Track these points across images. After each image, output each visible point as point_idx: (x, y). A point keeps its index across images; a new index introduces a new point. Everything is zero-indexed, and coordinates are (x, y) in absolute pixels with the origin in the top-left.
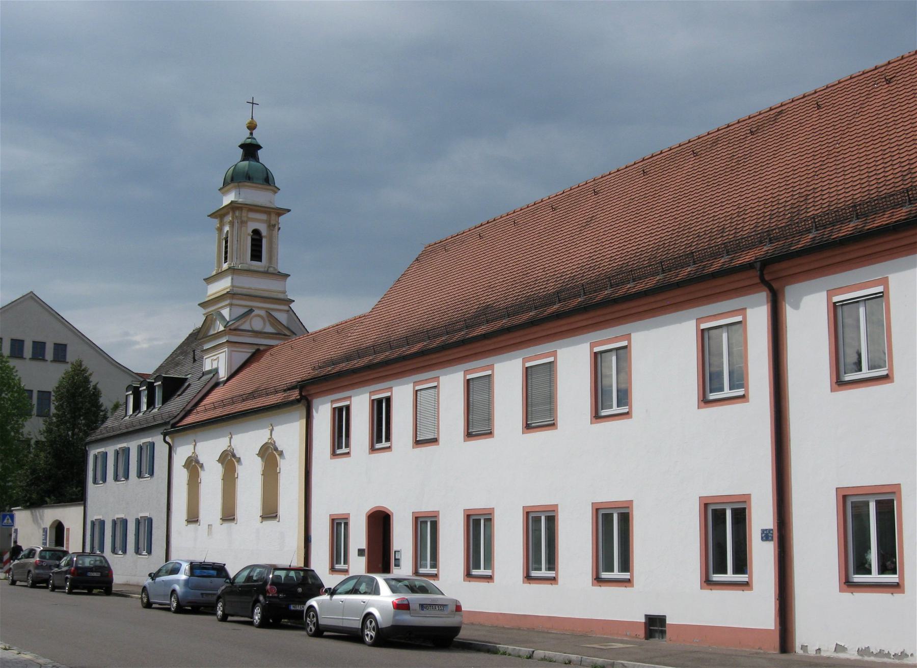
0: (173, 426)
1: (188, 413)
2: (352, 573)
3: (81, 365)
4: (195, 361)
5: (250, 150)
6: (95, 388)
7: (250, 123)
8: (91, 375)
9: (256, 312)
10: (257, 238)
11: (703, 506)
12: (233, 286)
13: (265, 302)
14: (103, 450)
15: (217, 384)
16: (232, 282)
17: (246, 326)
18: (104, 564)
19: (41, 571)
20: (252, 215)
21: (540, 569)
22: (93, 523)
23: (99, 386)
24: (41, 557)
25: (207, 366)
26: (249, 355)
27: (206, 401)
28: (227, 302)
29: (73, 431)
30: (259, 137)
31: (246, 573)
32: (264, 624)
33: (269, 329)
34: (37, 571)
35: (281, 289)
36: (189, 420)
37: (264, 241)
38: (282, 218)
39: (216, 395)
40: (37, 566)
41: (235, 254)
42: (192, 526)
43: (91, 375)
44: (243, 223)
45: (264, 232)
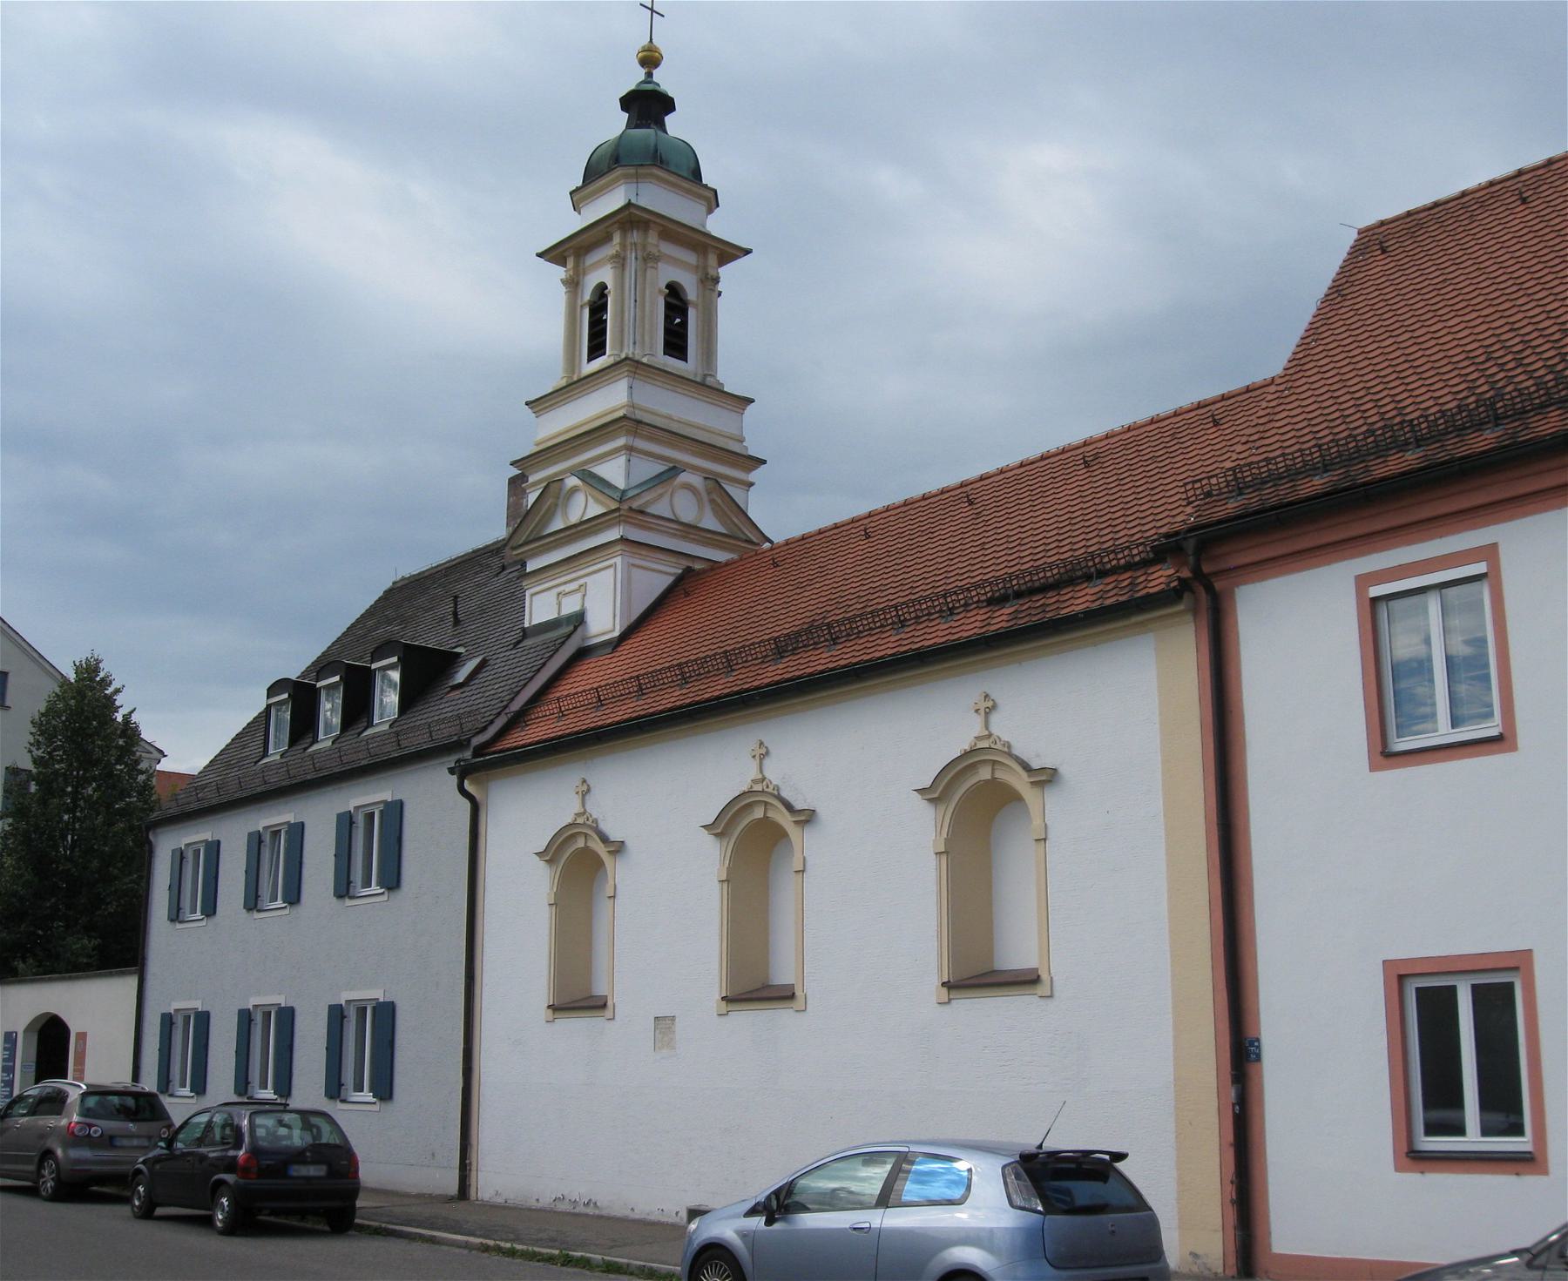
0: (479, 751)
2: (166, 1101)
3: (96, 670)
4: (457, 622)
5: (647, 105)
8: (118, 691)
9: (684, 477)
10: (676, 302)
11: (1395, 980)
12: (632, 406)
14: (290, 817)
15: (583, 653)
16: (631, 394)
17: (661, 508)
18: (327, 1137)
20: (667, 248)
21: (1460, 1130)
22: (168, 1021)
23: (134, 718)
24: (86, 1112)
25: (541, 607)
26: (670, 580)
28: (621, 442)
29: (74, 812)
30: (664, 79)
31: (204, 1118)
32: (232, 1229)
33: (710, 522)
34: (74, 1153)
35: (733, 431)
37: (692, 314)
38: (727, 273)
40: (74, 1139)
41: (629, 329)
43: (118, 691)
44: (649, 259)
45: (691, 292)
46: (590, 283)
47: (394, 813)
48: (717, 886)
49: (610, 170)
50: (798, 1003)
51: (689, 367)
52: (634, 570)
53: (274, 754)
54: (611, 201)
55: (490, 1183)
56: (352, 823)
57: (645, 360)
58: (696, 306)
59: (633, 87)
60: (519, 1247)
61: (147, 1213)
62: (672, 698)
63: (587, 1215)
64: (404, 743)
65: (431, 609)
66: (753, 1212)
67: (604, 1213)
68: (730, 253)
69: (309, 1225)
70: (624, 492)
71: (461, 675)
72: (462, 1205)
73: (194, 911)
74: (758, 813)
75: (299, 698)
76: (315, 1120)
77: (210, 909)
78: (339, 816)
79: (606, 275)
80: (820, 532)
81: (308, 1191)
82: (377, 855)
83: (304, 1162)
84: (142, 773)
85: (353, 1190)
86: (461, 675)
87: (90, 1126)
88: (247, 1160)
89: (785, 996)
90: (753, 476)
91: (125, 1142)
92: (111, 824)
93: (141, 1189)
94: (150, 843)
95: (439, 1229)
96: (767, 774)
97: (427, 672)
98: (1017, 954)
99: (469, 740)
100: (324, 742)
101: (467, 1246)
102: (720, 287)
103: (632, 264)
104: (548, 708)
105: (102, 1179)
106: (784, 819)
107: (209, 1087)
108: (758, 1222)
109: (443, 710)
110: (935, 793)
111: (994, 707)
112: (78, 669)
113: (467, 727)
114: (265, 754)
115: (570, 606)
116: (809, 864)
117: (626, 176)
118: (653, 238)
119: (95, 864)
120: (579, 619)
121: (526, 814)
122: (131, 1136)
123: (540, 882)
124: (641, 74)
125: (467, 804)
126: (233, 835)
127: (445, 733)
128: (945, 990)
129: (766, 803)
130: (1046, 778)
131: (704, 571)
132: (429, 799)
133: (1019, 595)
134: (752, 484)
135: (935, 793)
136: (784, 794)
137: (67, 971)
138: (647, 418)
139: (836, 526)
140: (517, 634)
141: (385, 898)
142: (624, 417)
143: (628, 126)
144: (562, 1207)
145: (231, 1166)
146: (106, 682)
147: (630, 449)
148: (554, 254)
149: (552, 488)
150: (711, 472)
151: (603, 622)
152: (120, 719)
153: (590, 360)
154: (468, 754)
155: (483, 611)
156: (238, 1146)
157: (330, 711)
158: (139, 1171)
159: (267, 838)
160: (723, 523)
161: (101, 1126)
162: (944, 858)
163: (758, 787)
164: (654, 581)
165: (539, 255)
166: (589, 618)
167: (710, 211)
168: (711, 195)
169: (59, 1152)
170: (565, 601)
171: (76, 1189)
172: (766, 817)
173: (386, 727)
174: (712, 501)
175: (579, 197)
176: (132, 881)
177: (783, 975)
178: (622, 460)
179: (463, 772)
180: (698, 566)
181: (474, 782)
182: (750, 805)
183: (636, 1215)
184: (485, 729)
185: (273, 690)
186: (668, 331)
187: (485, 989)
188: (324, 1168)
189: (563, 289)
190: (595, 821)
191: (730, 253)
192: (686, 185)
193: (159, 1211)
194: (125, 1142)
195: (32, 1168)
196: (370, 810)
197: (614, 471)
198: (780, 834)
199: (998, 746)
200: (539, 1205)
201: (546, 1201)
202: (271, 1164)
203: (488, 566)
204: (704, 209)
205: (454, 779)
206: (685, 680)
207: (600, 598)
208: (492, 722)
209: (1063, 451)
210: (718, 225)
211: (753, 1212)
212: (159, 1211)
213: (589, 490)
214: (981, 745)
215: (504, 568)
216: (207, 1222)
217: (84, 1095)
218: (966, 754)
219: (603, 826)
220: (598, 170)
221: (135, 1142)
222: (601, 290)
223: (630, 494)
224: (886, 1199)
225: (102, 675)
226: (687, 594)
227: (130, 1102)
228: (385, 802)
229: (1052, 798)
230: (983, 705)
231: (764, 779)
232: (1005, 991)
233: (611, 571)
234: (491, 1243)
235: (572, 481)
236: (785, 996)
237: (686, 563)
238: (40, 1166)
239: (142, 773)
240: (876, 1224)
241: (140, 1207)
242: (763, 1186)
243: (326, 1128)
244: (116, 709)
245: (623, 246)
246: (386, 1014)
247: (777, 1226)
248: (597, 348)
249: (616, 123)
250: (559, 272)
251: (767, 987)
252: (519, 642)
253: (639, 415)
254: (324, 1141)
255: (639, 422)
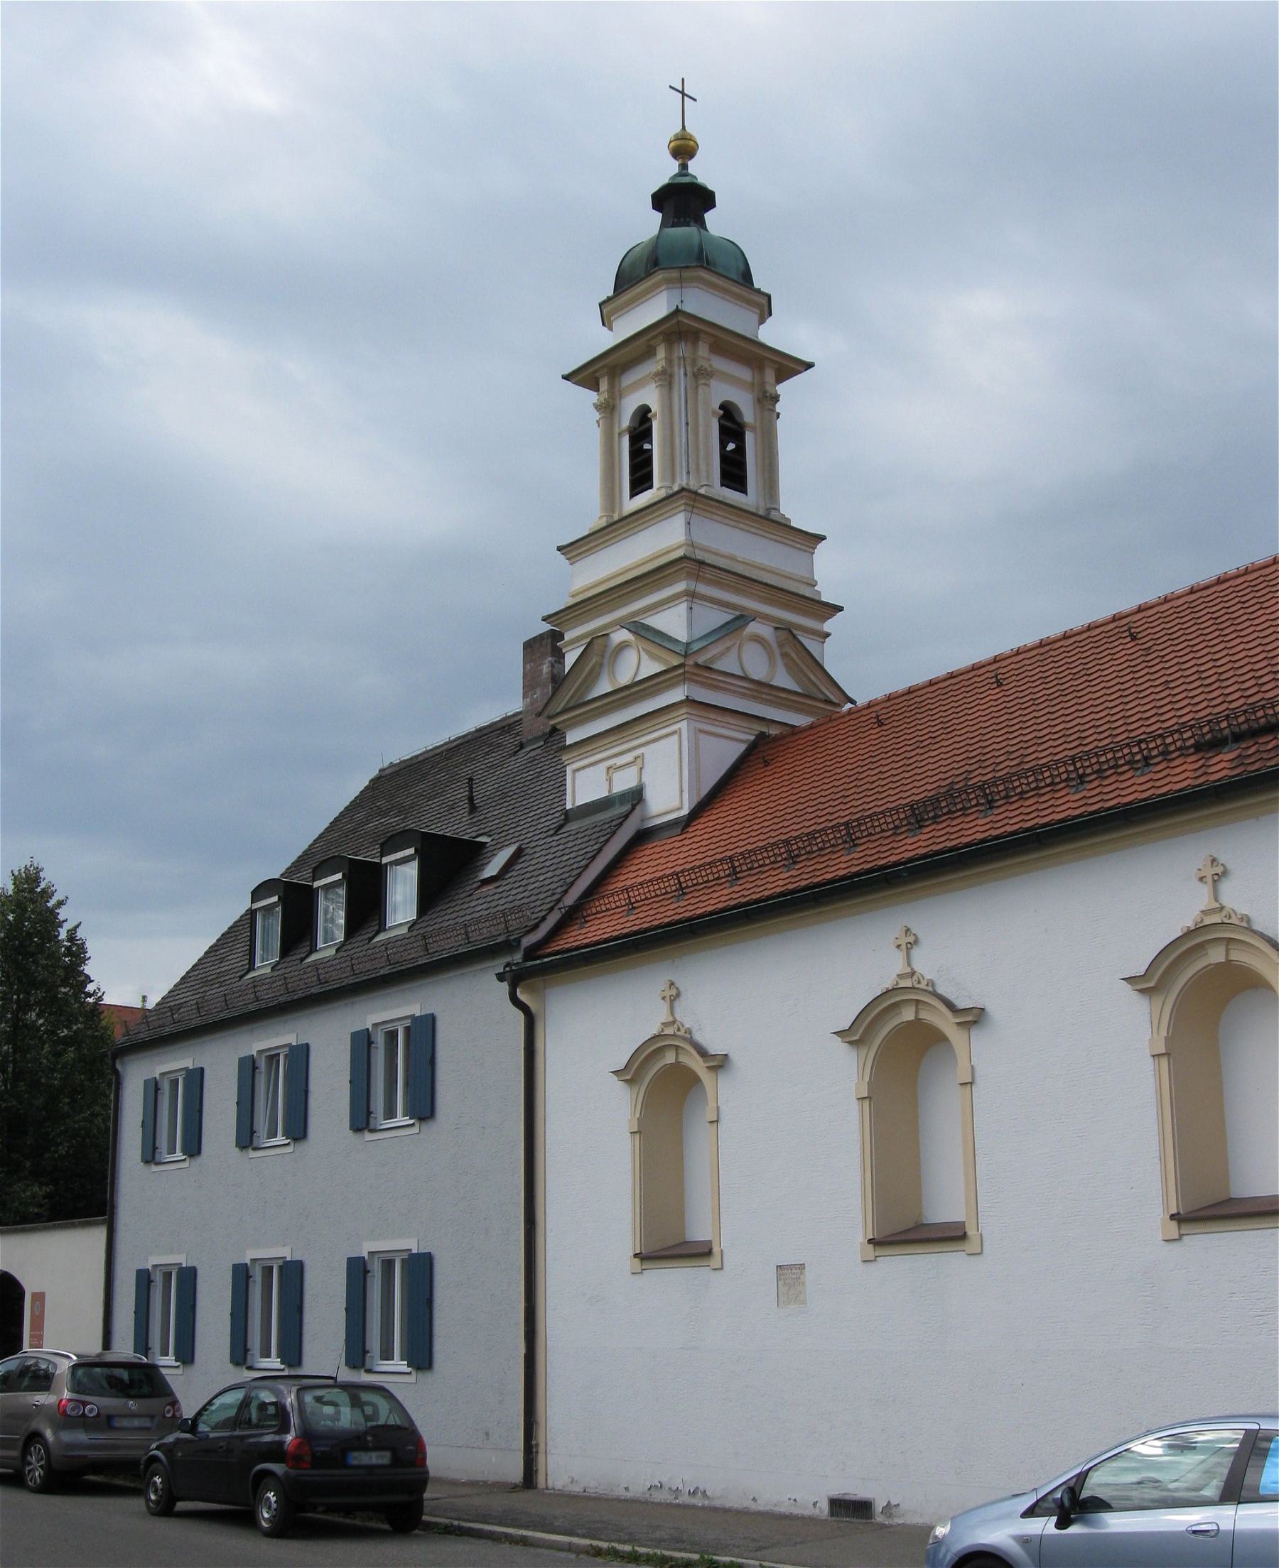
0: (531, 953)
1: (572, 916)
4: (473, 808)
5: (684, 201)
6: (72, 936)
7: (677, 138)
8: (60, 904)
9: (754, 628)
10: (731, 425)
12: (692, 545)
13: (771, 602)
14: (188, 1063)
17: (728, 664)
18: (385, 1415)
19: (82, 1437)
20: (719, 364)
22: (144, 1279)
23: (80, 934)
24: (77, 1387)
25: (587, 784)
27: (627, 877)
28: (681, 586)
30: (702, 170)
32: (282, 1530)
33: (783, 679)
34: (67, 1437)
36: (601, 927)
39: (650, 865)
40: (64, 1419)
42: (674, 1279)
43: (60, 904)
44: (701, 375)
45: (748, 414)
46: (629, 407)
47: (423, 1033)
48: (1149, 1064)
49: (648, 275)
50: (972, 1246)
51: (750, 499)
52: (702, 736)
53: (264, 966)
54: (653, 309)
55: (565, 1466)
56: (370, 1043)
57: (702, 491)
58: (753, 429)
59: (666, 181)
60: (642, 1550)
61: (165, 1509)
62: (778, 881)
63: (694, 1507)
64: (474, 937)
65: (435, 796)
66: (1030, 1513)
67: (717, 1503)
68: (790, 367)
69: (358, 1522)
70: (688, 644)
71: (491, 870)
72: (528, 1495)
73: (172, 1150)
74: (670, 1058)
75: (292, 901)
76: (365, 1397)
77: (193, 1147)
78: (146, 1082)
79: (650, 396)
80: (931, 683)
81: (366, 1479)
82: (406, 1079)
83: (365, 1449)
84: (90, 995)
85: (421, 1481)
86: (491, 870)
87: (85, 1404)
88: (299, 1446)
89: (701, 1253)
90: (828, 626)
91: (125, 1423)
92: (58, 1055)
93: (158, 1480)
94: (117, 1073)
95: (527, 1528)
96: (917, 966)
97: (447, 867)
98: (945, 1207)
99: (518, 941)
100: (325, 950)
101: (570, 1548)
102: (779, 407)
103: (681, 381)
104: (613, 899)
105: (98, 1466)
106: (697, 1064)
107: (197, 1356)
108: (1045, 1526)
109: (475, 909)
110: (1149, 983)
111: (1225, 873)
112: (16, 880)
113: (514, 925)
114: (251, 967)
115: (624, 782)
116: (722, 1116)
117: (668, 281)
118: (703, 350)
119: (40, 1102)
120: (636, 797)
121: (593, 1030)
122: (133, 1415)
123: (618, 1109)
124: (673, 167)
125: (520, 1016)
126: (219, 1061)
127: (483, 935)
128: (1174, 1223)
129: (677, 1047)
130: (974, 1018)
131: (776, 739)
132: (470, 1015)
133: (1238, 737)
134: (828, 635)
135: (1149, 983)
136: (941, 990)
137: (15, 1223)
138: (709, 559)
139: (952, 676)
140: (558, 818)
141: (415, 1130)
142: (683, 558)
143: (664, 224)
144: (659, 1497)
145: (276, 1453)
146: (47, 894)
147: (691, 595)
148: (585, 376)
149: (595, 643)
150: (779, 620)
151: (667, 797)
152: (63, 934)
153: (632, 495)
154: (518, 957)
155: (505, 796)
156: (285, 1429)
157: (332, 915)
158: (154, 1459)
159: (262, 1064)
160: (798, 682)
161: (98, 1404)
162: (866, 1103)
163: (907, 983)
164: (725, 750)
165: (566, 377)
166: (649, 794)
167: (762, 321)
168: (764, 301)
169: (49, 1434)
170: (617, 776)
171: (68, 1478)
172: (918, 1020)
173: (332, 952)
174: (785, 655)
175: (608, 311)
176: (85, 1119)
177: (699, 1231)
178: (682, 608)
179: (515, 978)
180: (773, 731)
181: (531, 990)
182: (896, 1005)
183: (761, 1506)
184: (536, 927)
185: (257, 894)
186: (725, 458)
187: (550, 1236)
188: (388, 1454)
189: (597, 415)
190: (689, 1031)
191: (790, 367)
192: (736, 289)
193: (181, 1506)
194: (125, 1423)
195: (15, 1453)
196: (390, 1027)
197: (674, 622)
198: (693, 1080)
199: (922, 986)
200: (629, 1495)
201: (638, 1489)
202: (326, 1451)
203: (500, 745)
204: (756, 318)
205: (505, 987)
206: (793, 859)
207: (665, 773)
208: (544, 918)
209: (1247, 572)
210: (771, 334)
211: (1030, 1513)
212: (181, 1506)
213: (643, 645)
214: (1208, 921)
215: (522, 746)
216: (246, 1519)
217: (75, 1367)
218: (1189, 934)
219: (698, 1037)
220: (632, 276)
221: (136, 1423)
222: (643, 415)
223: (696, 647)
224: (1236, 1490)
225: (43, 885)
226: (767, 764)
227: (124, 1375)
228: (289, 1045)
229: (978, 1039)
230: (1210, 872)
231: (913, 973)
232: (929, 1248)
233: (676, 737)
234: (604, 1545)
235: (621, 635)
236: (701, 1253)
237: (759, 728)
238: (26, 1450)
239: (90, 995)
240: (1226, 1526)
241: (157, 1502)
242: (1054, 1479)
243: (383, 1406)
244: (60, 925)
245: (669, 360)
246: (420, 1269)
247: (1074, 1529)
248: (641, 480)
249: (649, 224)
250: (588, 398)
251: (920, 1226)
252: (561, 827)
253: (700, 555)
254: (381, 1422)
255: (702, 563)
